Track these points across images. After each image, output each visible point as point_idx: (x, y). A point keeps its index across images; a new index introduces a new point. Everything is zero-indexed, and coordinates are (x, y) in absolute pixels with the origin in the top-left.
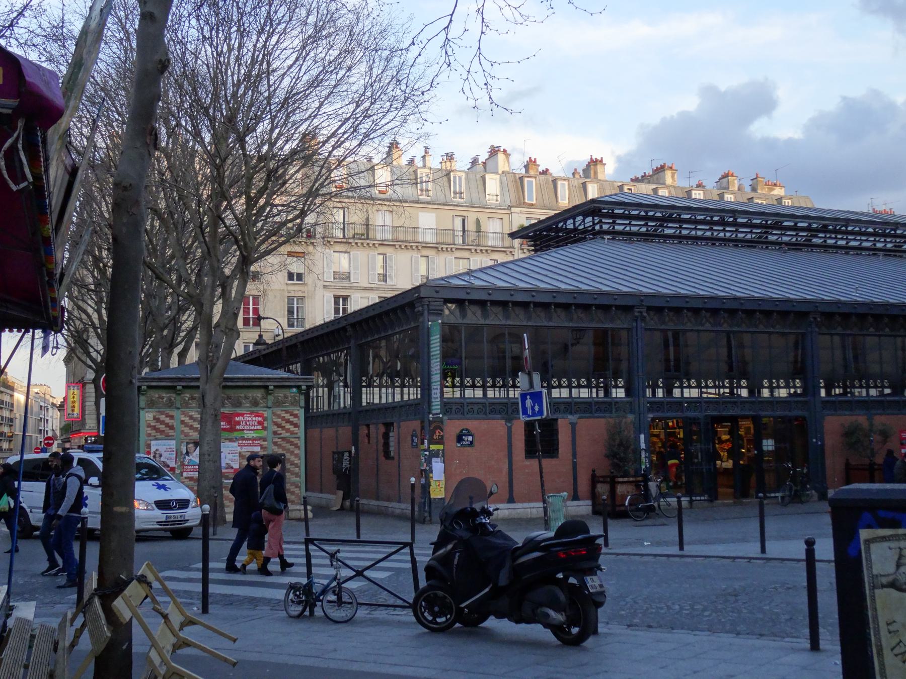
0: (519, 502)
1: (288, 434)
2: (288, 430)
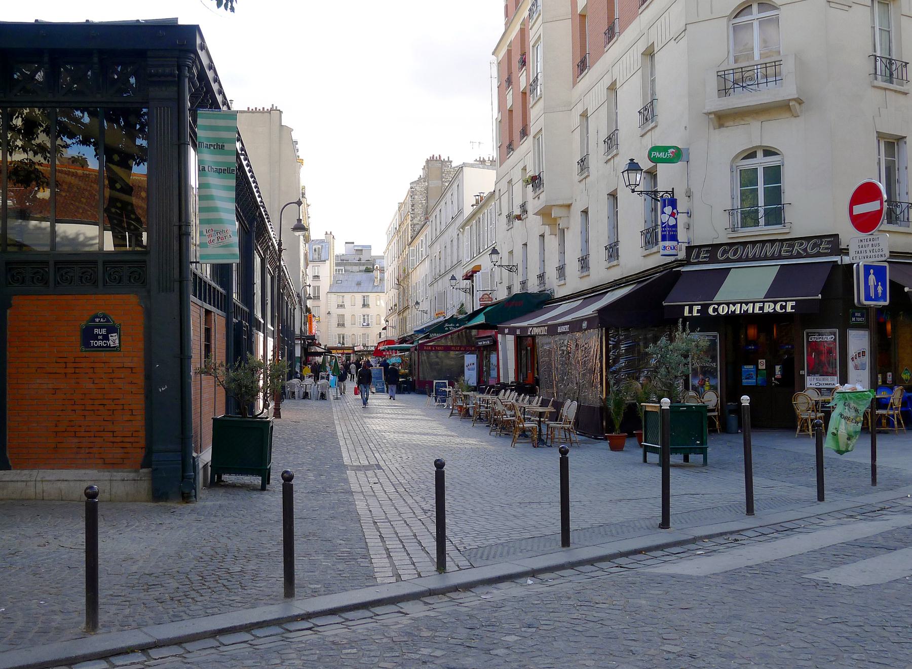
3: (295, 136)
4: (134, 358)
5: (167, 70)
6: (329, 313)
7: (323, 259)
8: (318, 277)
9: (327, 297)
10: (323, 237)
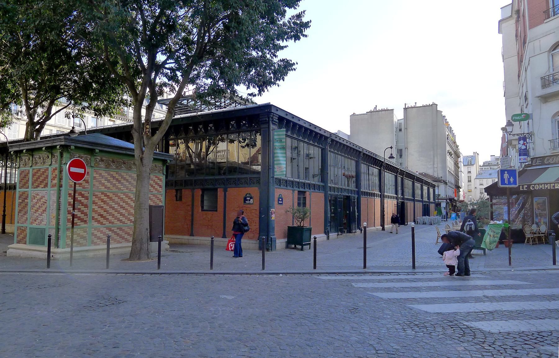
0: (196, 236)
1: (156, 192)
2: (156, 189)
3: (443, 114)
4: (256, 206)
5: (265, 119)
6: (476, 188)
7: (472, 164)
8: (470, 172)
9: (475, 182)
10: (472, 154)
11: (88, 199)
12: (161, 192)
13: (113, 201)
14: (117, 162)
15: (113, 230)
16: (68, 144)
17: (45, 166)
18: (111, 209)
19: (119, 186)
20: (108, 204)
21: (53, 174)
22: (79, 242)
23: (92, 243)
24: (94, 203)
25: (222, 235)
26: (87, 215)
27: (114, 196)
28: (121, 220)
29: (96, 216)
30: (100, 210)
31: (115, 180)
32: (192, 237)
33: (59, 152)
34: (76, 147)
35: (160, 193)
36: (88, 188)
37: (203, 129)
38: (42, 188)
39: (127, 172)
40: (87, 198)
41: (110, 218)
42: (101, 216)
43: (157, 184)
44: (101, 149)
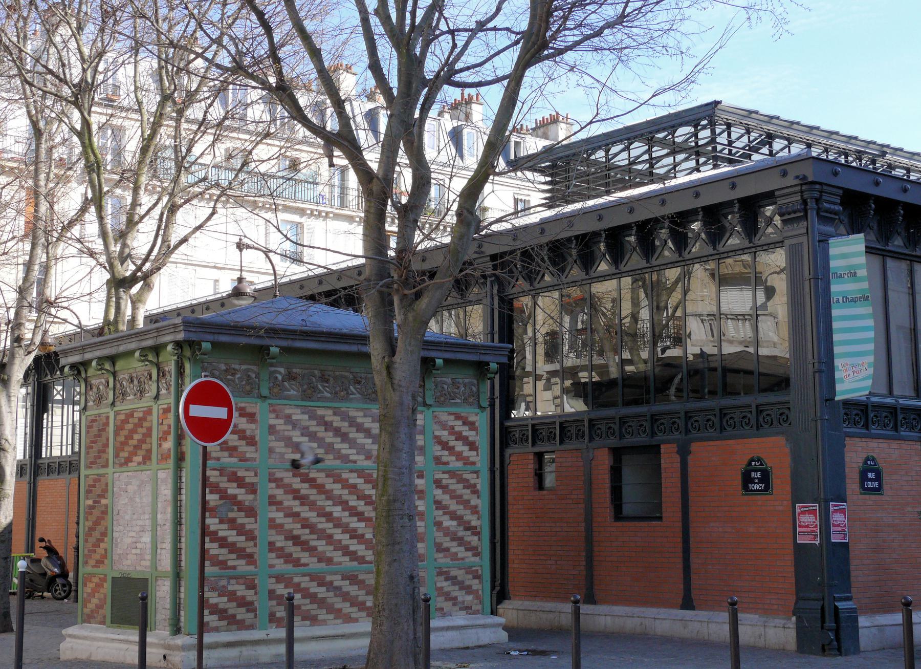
1: (459, 464)
2: (459, 456)
11: (254, 492)
12: (474, 463)
13: (329, 495)
14: (335, 378)
15: (331, 583)
16: (193, 337)
17: (147, 401)
18: (323, 519)
19: (344, 448)
20: (312, 505)
21: (162, 424)
22: (234, 616)
23: (271, 621)
24: (273, 501)
25: (680, 601)
26: (254, 538)
27: (331, 480)
28: (355, 553)
29: (280, 541)
30: (290, 524)
31: (331, 434)
32: (688, 614)
33: (173, 362)
34: (214, 344)
35: (473, 468)
36: (254, 459)
37: (670, 244)
38: (139, 464)
39: (366, 406)
40: (252, 489)
41: (321, 545)
42: (296, 540)
43: (459, 437)
44: (284, 343)
